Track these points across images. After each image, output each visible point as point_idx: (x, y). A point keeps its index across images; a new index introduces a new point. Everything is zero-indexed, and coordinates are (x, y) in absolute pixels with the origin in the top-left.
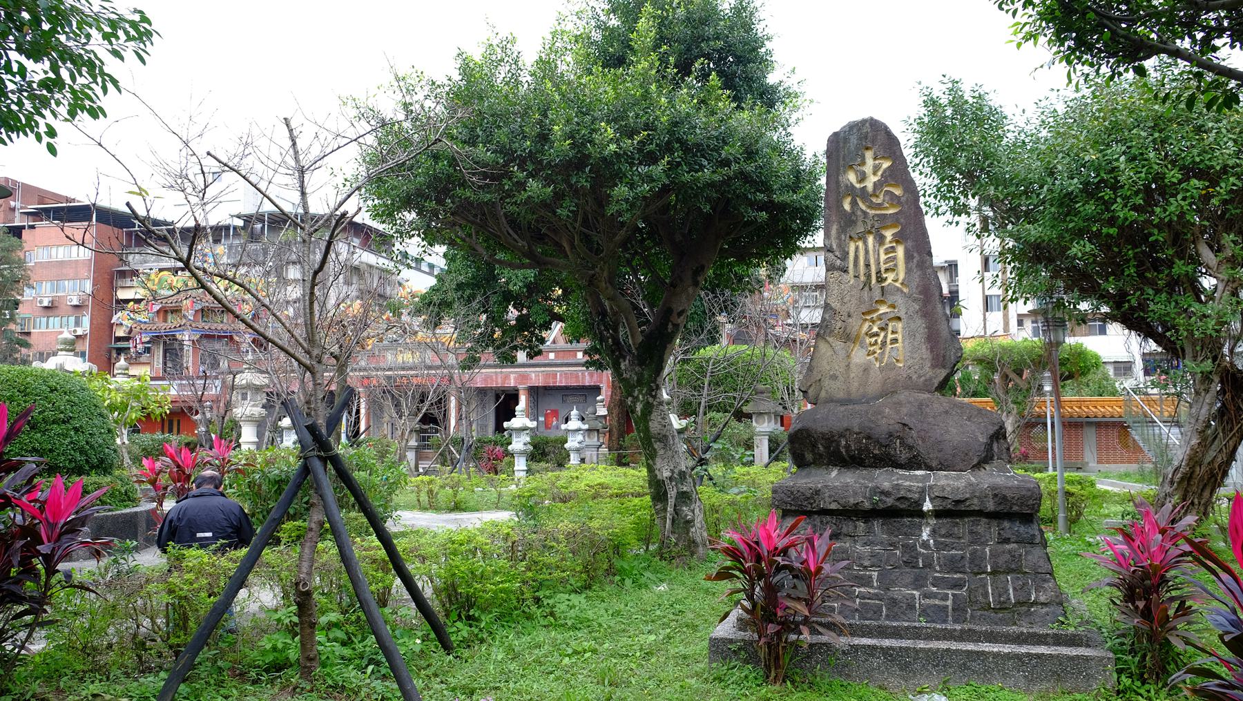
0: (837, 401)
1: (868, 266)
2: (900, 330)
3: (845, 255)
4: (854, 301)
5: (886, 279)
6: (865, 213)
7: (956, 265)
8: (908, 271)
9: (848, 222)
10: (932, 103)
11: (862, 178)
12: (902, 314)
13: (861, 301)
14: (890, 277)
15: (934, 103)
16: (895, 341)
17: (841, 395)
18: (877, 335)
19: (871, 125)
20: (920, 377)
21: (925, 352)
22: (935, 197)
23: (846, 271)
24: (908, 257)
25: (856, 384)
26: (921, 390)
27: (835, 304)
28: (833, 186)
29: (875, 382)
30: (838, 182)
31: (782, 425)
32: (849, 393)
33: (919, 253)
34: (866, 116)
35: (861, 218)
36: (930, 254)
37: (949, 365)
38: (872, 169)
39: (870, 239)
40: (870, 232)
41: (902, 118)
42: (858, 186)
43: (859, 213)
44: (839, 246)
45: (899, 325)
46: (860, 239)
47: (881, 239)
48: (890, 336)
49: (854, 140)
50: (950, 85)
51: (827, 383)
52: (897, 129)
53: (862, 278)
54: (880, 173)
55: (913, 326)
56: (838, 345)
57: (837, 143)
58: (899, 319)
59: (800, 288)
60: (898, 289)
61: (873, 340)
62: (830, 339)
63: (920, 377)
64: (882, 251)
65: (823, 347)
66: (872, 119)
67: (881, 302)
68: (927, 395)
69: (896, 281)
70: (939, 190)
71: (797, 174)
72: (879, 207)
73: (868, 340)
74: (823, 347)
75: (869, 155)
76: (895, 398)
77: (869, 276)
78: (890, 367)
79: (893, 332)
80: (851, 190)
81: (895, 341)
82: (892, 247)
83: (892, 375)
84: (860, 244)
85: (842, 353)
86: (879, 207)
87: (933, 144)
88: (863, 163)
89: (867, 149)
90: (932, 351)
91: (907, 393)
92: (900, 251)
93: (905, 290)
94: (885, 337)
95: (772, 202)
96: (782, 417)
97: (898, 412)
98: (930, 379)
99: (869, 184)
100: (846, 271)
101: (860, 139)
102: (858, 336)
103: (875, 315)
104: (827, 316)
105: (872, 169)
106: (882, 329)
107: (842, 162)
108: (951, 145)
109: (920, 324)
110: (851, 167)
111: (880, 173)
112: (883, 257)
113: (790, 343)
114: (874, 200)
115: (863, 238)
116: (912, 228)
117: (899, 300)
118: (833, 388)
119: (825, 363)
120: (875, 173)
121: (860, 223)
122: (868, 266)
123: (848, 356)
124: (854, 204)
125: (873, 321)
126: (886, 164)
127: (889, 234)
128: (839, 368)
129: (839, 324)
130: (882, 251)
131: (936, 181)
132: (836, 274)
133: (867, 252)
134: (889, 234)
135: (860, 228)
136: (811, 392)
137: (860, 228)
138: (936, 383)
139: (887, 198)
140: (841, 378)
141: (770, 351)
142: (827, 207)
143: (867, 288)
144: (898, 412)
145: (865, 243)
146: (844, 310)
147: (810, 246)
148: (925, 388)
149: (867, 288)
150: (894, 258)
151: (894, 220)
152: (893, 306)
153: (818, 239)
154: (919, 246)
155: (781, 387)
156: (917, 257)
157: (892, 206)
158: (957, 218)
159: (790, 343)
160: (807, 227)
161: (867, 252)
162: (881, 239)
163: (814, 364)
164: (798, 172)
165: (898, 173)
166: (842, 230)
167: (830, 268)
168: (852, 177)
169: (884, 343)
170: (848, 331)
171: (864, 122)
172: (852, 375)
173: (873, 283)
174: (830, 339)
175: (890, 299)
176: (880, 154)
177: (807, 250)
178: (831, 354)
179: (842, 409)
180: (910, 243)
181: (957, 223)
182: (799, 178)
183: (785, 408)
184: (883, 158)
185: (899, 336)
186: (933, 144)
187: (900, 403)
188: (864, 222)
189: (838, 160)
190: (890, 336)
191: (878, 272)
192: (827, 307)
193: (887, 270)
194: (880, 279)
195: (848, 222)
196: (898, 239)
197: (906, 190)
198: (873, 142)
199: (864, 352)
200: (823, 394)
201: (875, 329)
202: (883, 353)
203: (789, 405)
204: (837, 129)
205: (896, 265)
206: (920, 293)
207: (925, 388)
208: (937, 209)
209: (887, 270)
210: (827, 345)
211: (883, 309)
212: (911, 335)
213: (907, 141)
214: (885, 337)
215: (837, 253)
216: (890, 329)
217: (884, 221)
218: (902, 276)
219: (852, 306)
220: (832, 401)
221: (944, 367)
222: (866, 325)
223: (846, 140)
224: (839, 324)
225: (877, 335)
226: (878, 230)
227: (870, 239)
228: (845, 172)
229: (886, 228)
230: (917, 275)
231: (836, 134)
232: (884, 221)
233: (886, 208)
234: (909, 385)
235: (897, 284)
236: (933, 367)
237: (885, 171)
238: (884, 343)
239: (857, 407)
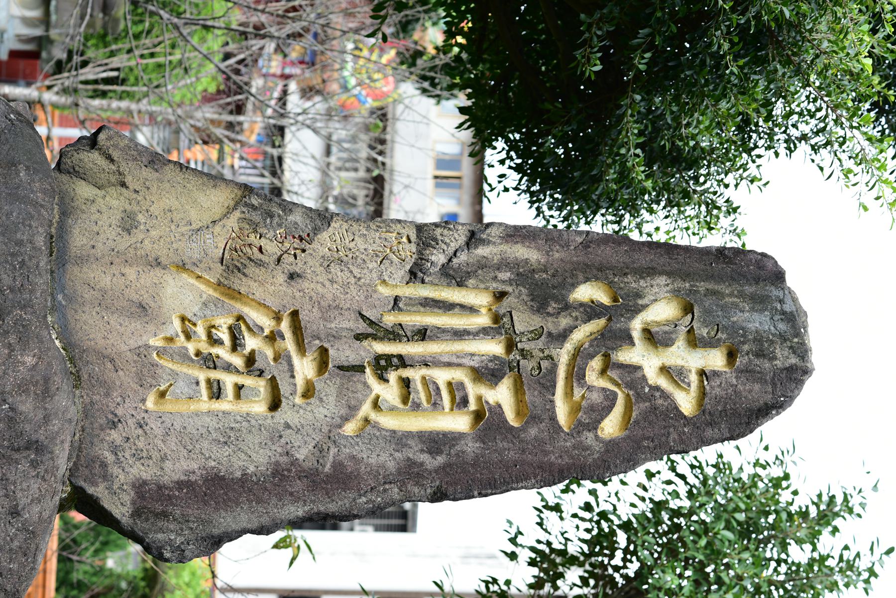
0: (62, 227)
1: (422, 334)
2: (244, 407)
3: (454, 276)
4: (330, 292)
5: (383, 379)
6: (563, 336)
7: (403, 529)
8: (399, 439)
9: (546, 291)
10: (827, 514)
11: (655, 338)
12: (285, 414)
13: (330, 309)
14: (390, 392)
15: (825, 518)
16: (216, 392)
17: (78, 240)
18: (236, 345)
19: (791, 369)
20: (115, 450)
21: (178, 468)
22: (588, 507)
23: (415, 275)
24: (436, 442)
25: (106, 281)
26: (78, 450)
27: (325, 243)
28: (644, 259)
29: (105, 332)
30: (650, 272)
31: (13, 54)
32: (82, 260)
33: (443, 469)
34: (816, 358)
35: (550, 325)
36: (438, 496)
37: (140, 526)
38: (678, 365)
39: (494, 348)
40: (510, 346)
41: (799, 448)
42: (636, 326)
43: (564, 321)
44: (483, 264)
45: (259, 408)
46: (497, 318)
47: (488, 373)
48: (229, 381)
49: (758, 322)
50: (863, 564)
51: (114, 203)
52: (774, 431)
53: (390, 320)
54: (663, 383)
55: (253, 440)
56: (216, 243)
57: (756, 274)
58: (275, 405)
59: (380, 124)
60: (353, 409)
61: (225, 337)
62: (233, 221)
63: (115, 450)
64: (458, 375)
65: (217, 199)
66: (807, 372)
67: (323, 363)
68: (63, 464)
69: (376, 405)
70: (603, 515)
71: (691, 161)
72: (576, 374)
73: (224, 322)
74: (217, 199)
75: (716, 359)
76: (59, 381)
77: (394, 334)
78: (146, 372)
79: (239, 388)
80: (628, 304)
81: (216, 392)
82: (465, 402)
83: (125, 378)
84: (484, 320)
85: (192, 251)
86: (576, 374)
87: (720, 511)
88: (694, 341)
89: (731, 356)
90: (180, 485)
91: (74, 412)
92: (459, 423)
93: (350, 428)
94: (229, 368)
95: (623, 90)
96: (34, 56)
97: (22, 388)
98: (106, 477)
99: (636, 354)
100: (415, 275)
101: (759, 339)
102: (235, 294)
103: (289, 344)
104: (296, 217)
105: (678, 365)
106: (250, 360)
107: (702, 286)
108: (714, 553)
109: (255, 458)
110: (688, 309)
111: (663, 383)
112: (442, 376)
113: (232, 95)
114: (596, 363)
115: (500, 324)
116: (512, 455)
117: (325, 410)
118: (98, 213)
119: (169, 201)
120: (665, 370)
121: (536, 322)
122: (422, 334)
123: (182, 267)
124: (592, 311)
125: (273, 337)
126: (686, 403)
127: (502, 395)
128: (153, 238)
129: (272, 248)
130: (458, 375)
131: (625, 513)
132: (409, 251)
133: (460, 334)
134: (502, 395)
135: (524, 321)
136: (92, 159)
137: (524, 321)
138: (98, 491)
139: (596, 397)
140: (125, 242)
141: (214, 43)
142: (590, 240)
143: (362, 327)
144: (22, 388)
145: (484, 332)
146: (308, 263)
147: (491, 174)
148: (84, 461)
149: (362, 327)
150: (436, 405)
151: (537, 414)
152: (309, 392)
153: (510, 205)
154: (462, 475)
155: (115, 62)
156: (431, 462)
157: (575, 409)
158: (525, 555)
159: (232, 95)
160: (543, 176)
161: (460, 334)
162: (488, 373)
163: (169, 172)
164: (693, 163)
165: (657, 431)
166: (524, 275)
167: (425, 235)
168: (661, 310)
169: (210, 362)
170: (251, 270)
171: (802, 351)
172: (131, 273)
173: (383, 348)
174: (233, 221)
175: (328, 388)
176: (715, 389)
177: (477, 156)
178: (197, 217)
179: (40, 241)
180: (471, 447)
181: (513, 556)
182: (676, 169)
183: (59, 67)
184: (703, 393)
185: (226, 405)
186: (720, 511)
187: (46, 393)
188: (537, 334)
189: (710, 277)
190: (229, 381)
191: (403, 362)
192: (322, 218)
193: (406, 383)
194: (383, 366)
195: (546, 291)
196: (486, 419)
197: (611, 445)
198: (747, 372)
199: (192, 309)
200: (84, 190)
201: (251, 343)
202: (184, 356)
203: (67, 79)
204: (791, 281)
205: (417, 406)
206: (338, 466)
207: (84, 461)
208: (557, 508)
209: (406, 383)
210: (218, 211)
211: (305, 368)
212: (229, 434)
213: (741, 454)
214: (229, 368)
215: (463, 257)
216: (249, 381)
217: (536, 384)
218: (388, 422)
219: (319, 285)
220: (64, 214)
221: (137, 513)
222: (267, 323)
223: (760, 302)
224: (272, 248)
225: (236, 345)
226: (514, 368)
227: (494, 348)
228: (676, 293)
229: (518, 388)
230: (387, 459)
231: (778, 276)
232: (536, 384)
233: (569, 393)
234: (95, 421)
235: (366, 409)
236: (140, 487)
237: (666, 396)
238: (210, 362)
239: (42, 281)
